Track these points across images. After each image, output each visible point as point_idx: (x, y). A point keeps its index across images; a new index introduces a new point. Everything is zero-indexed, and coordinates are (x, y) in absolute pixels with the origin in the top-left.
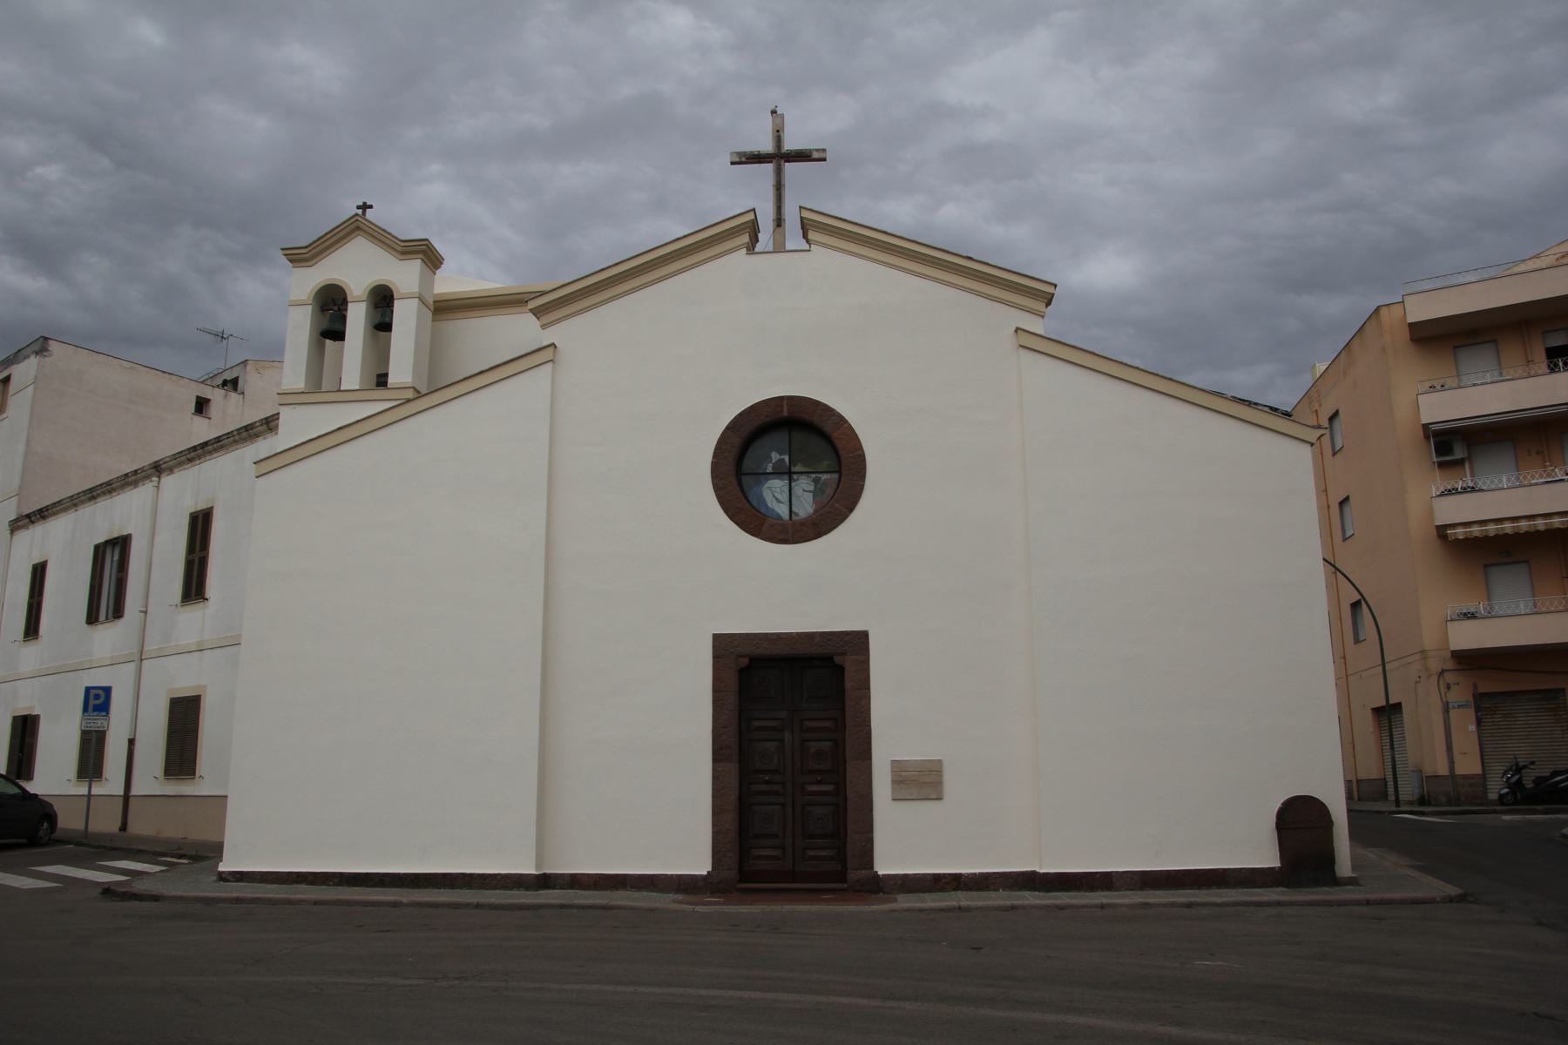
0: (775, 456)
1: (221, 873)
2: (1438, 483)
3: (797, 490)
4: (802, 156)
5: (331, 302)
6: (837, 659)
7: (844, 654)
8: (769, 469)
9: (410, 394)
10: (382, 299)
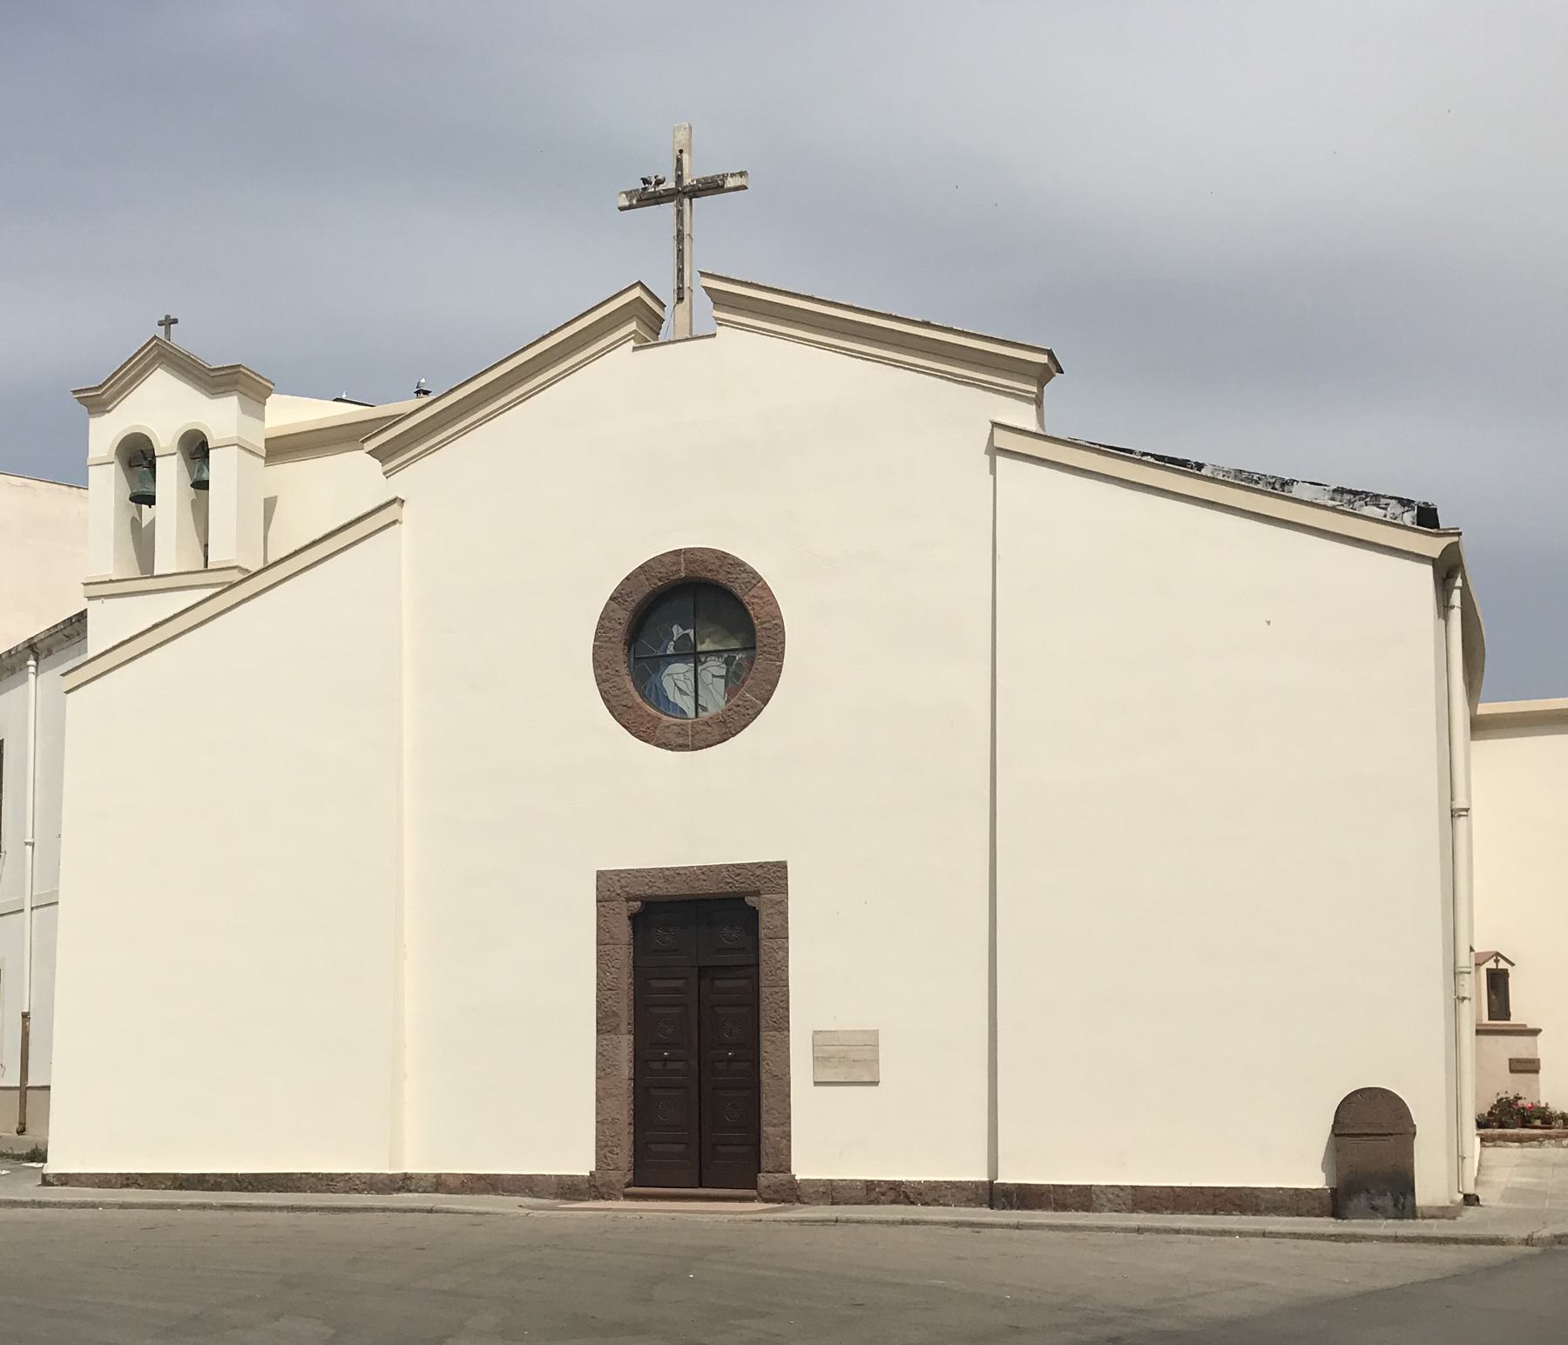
0: (677, 631)
1: (44, 1176)
2: (666, 314)
3: (705, 676)
4: (713, 186)
5: (138, 455)
6: (750, 900)
7: (757, 893)
8: (670, 650)
9: (236, 576)
10: (196, 449)
